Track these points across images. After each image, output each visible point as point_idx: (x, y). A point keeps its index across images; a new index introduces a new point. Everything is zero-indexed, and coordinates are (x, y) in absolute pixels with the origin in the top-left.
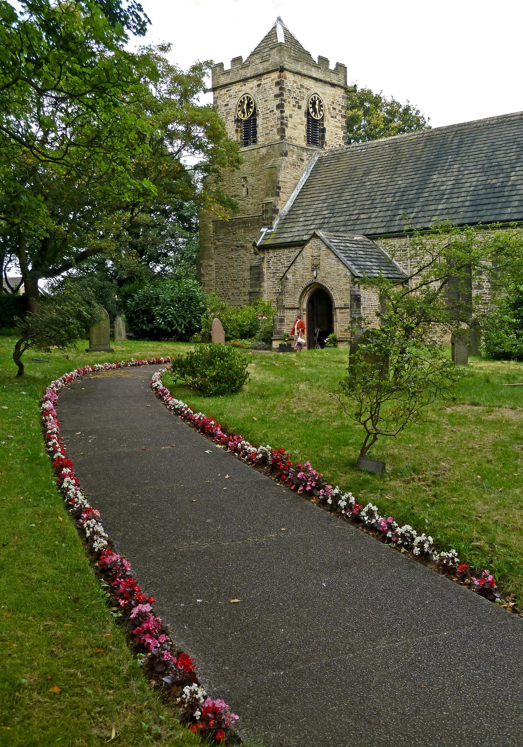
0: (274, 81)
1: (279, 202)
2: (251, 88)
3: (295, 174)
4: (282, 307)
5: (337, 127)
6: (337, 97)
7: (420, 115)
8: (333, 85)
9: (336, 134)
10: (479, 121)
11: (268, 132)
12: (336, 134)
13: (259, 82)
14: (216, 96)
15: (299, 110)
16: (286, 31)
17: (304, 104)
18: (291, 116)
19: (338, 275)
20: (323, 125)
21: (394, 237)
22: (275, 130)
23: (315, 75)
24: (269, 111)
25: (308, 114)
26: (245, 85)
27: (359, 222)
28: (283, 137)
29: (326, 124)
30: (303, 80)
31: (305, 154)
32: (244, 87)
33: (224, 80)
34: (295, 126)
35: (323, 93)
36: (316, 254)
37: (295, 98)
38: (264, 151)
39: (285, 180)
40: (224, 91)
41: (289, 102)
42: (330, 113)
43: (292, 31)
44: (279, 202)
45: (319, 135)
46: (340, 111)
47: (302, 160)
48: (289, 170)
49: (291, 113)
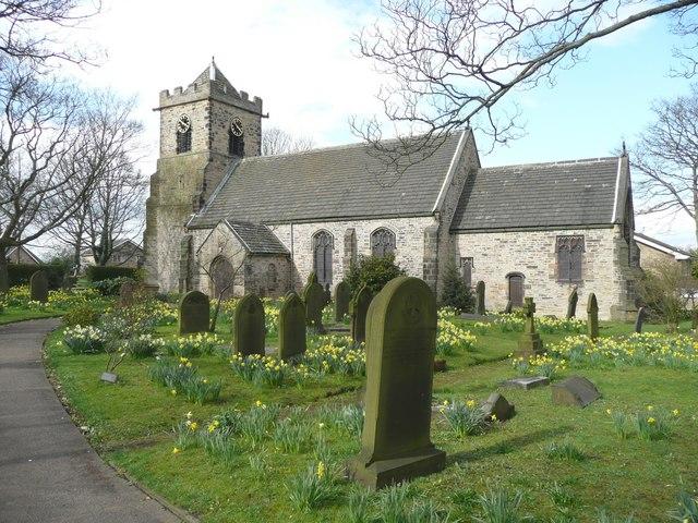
7: (648, 135)
8: (251, 112)
10: (528, 170)
16: (218, 73)
17: (227, 125)
21: (315, 261)
25: (230, 132)
28: (139, 268)
33: (168, 102)
38: (196, 157)
40: (168, 111)
43: (219, 67)
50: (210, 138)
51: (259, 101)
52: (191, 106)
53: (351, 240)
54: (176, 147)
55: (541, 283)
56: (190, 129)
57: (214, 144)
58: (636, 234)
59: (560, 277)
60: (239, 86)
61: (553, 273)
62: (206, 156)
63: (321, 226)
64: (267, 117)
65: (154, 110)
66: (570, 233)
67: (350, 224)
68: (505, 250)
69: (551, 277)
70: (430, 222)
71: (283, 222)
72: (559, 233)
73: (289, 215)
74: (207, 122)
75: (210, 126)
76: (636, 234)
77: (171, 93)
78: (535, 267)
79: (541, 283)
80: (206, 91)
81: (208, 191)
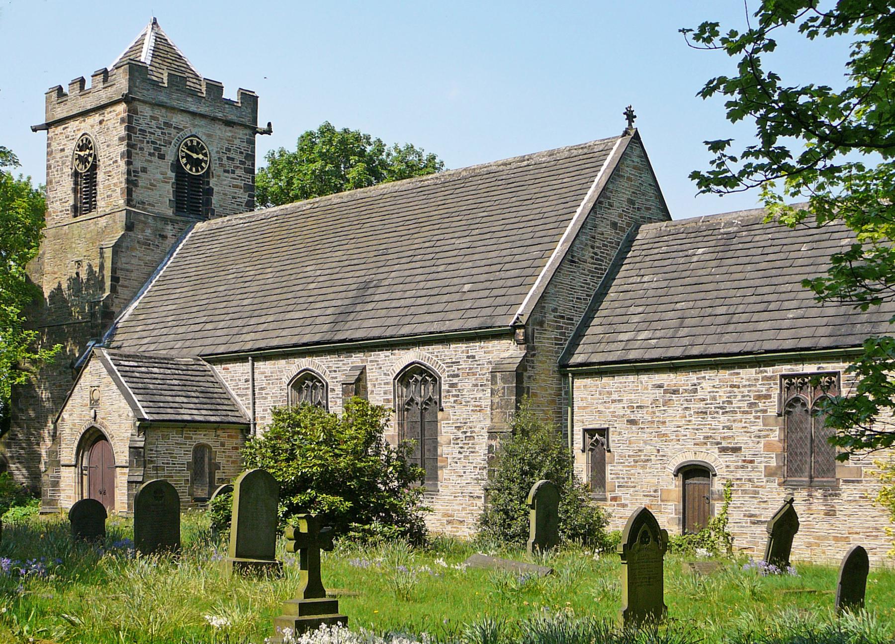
0: (120, 117)
1: (116, 301)
2: (92, 126)
3: (149, 258)
4: (55, 463)
5: (235, 186)
6: (237, 142)
8: (229, 123)
9: (234, 198)
11: (109, 193)
12: (234, 198)
13: (101, 118)
14: (50, 135)
15: (160, 161)
16: (160, 40)
18: (144, 170)
19: (120, 416)
20: (208, 183)
22: (118, 190)
23: (193, 108)
24: (111, 162)
25: (177, 167)
26: (84, 121)
27: (731, 328)
29: (213, 182)
30: (169, 115)
31: (170, 227)
32: (83, 124)
33: (61, 112)
34: (152, 185)
35: (209, 136)
36: (96, 384)
37: (153, 143)
39: (128, 267)
40: (60, 129)
41: (141, 149)
42: (221, 165)
44: (116, 301)
45: (202, 198)
46: (242, 162)
47: (164, 237)
48: (138, 254)
49: (145, 165)
50: (128, 181)
51: (250, 100)
52: (97, 118)
53: (358, 385)
54: (72, 202)
55: (748, 486)
56: (208, 172)
57: (138, 195)
58: (82, 497)
59: (789, 470)
60: (204, 65)
61: (773, 463)
62: (121, 217)
63: (305, 363)
64: (269, 131)
65: (35, 130)
66: (810, 368)
67: (357, 359)
68: (674, 414)
69: (770, 473)
70: (508, 351)
71: (238, 357)
72: (786, 369)
73: (248, 341)
74: (123, 148)
75: (128, 156)
76: (82, 497)
77: (66, 90)
78: (736, 450)
79: (748, 486)
80: (121, 83)
81: (123, 293)
